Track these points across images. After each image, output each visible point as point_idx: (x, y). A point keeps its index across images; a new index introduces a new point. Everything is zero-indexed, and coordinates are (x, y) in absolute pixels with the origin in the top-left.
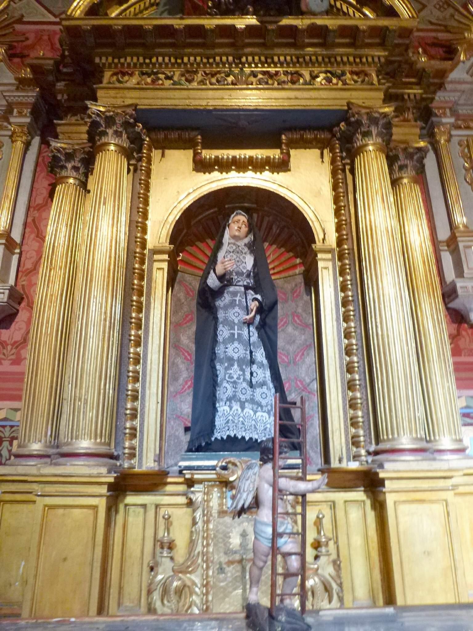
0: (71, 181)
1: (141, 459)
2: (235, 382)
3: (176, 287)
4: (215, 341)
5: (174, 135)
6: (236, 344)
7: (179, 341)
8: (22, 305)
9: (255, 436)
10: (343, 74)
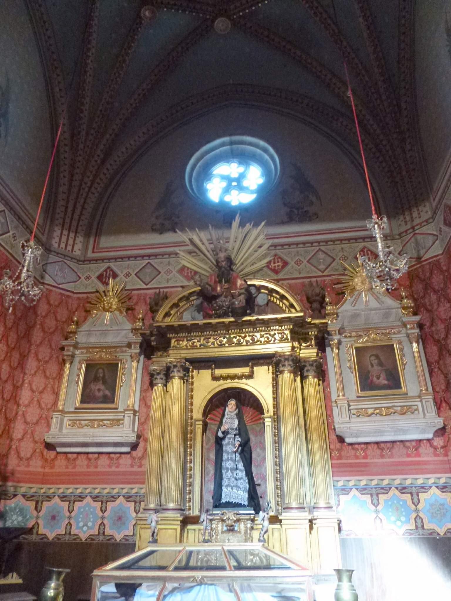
1: (193, 511)
2: (229, 479)
3: (207, 431)
4: (222, 460)
6: (230, 462)
8: (141, 439)
10: (275, 334)
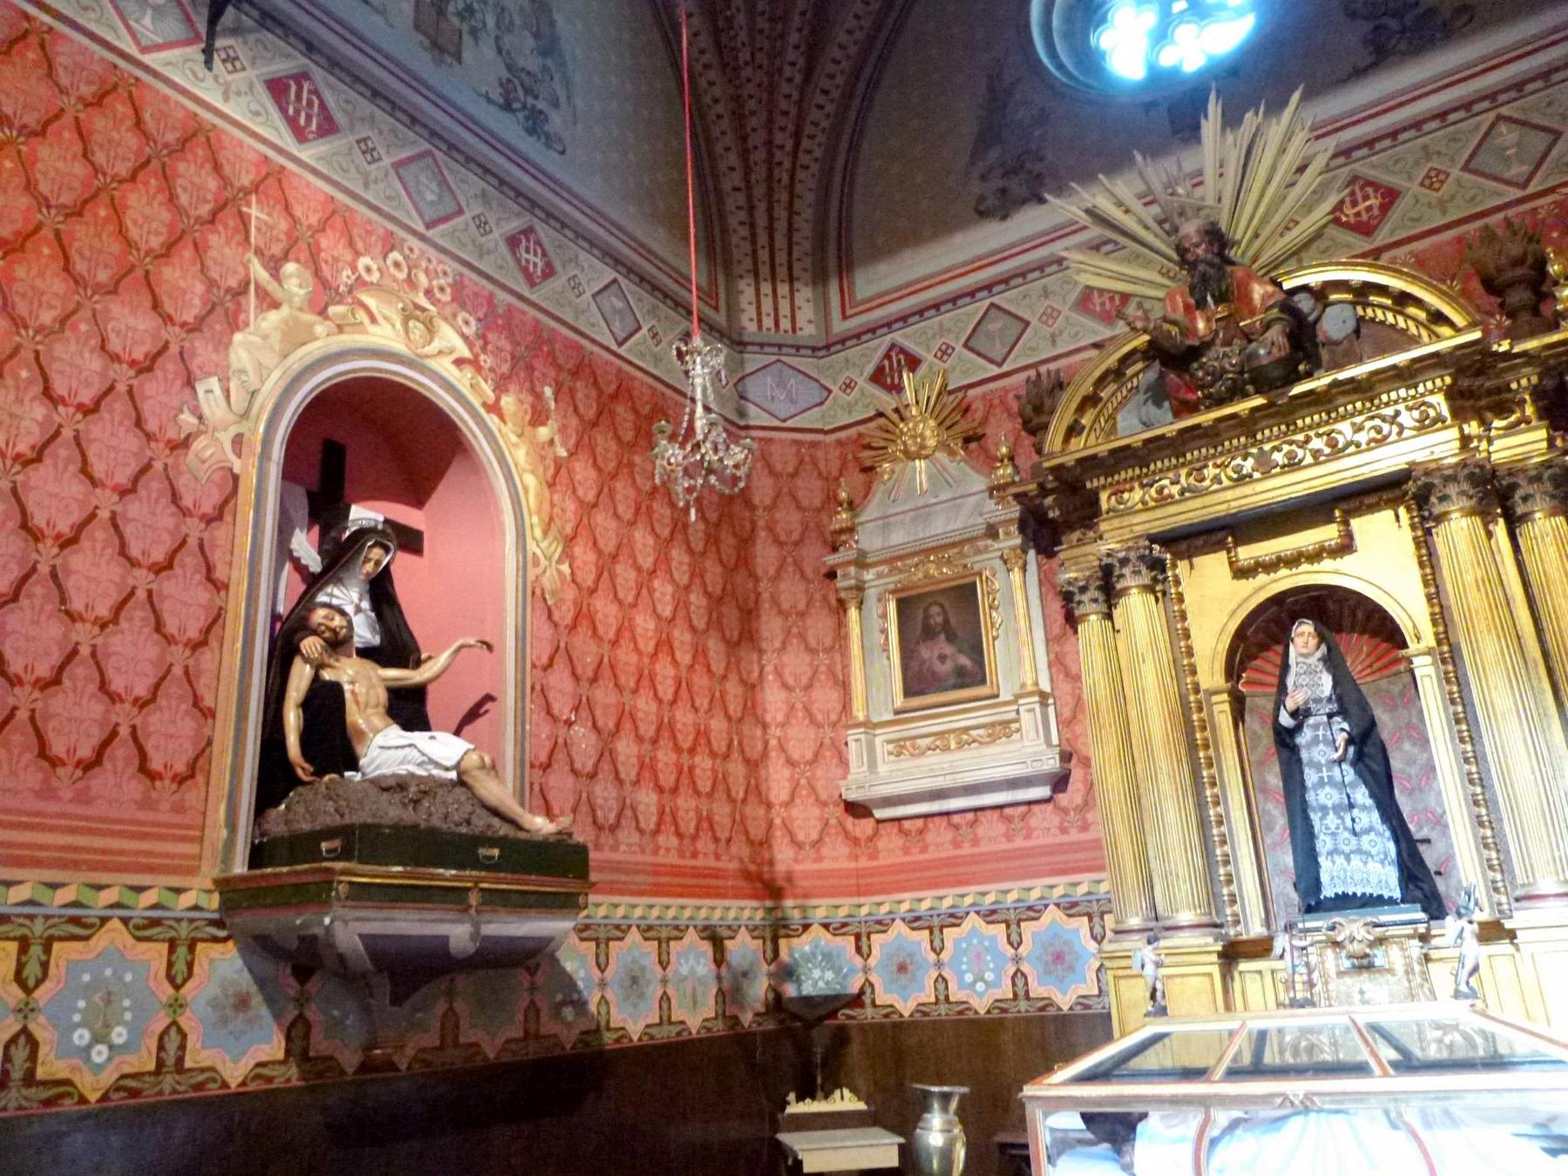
0: (1093, 618)
1: (1246, 925)
2: (1334, 834)
3: (1247, 718)
4: (1303, 787)
5: (1200, 542)
7: (1265, 782)
9: (1368, 891)
10: (1398, 413)
